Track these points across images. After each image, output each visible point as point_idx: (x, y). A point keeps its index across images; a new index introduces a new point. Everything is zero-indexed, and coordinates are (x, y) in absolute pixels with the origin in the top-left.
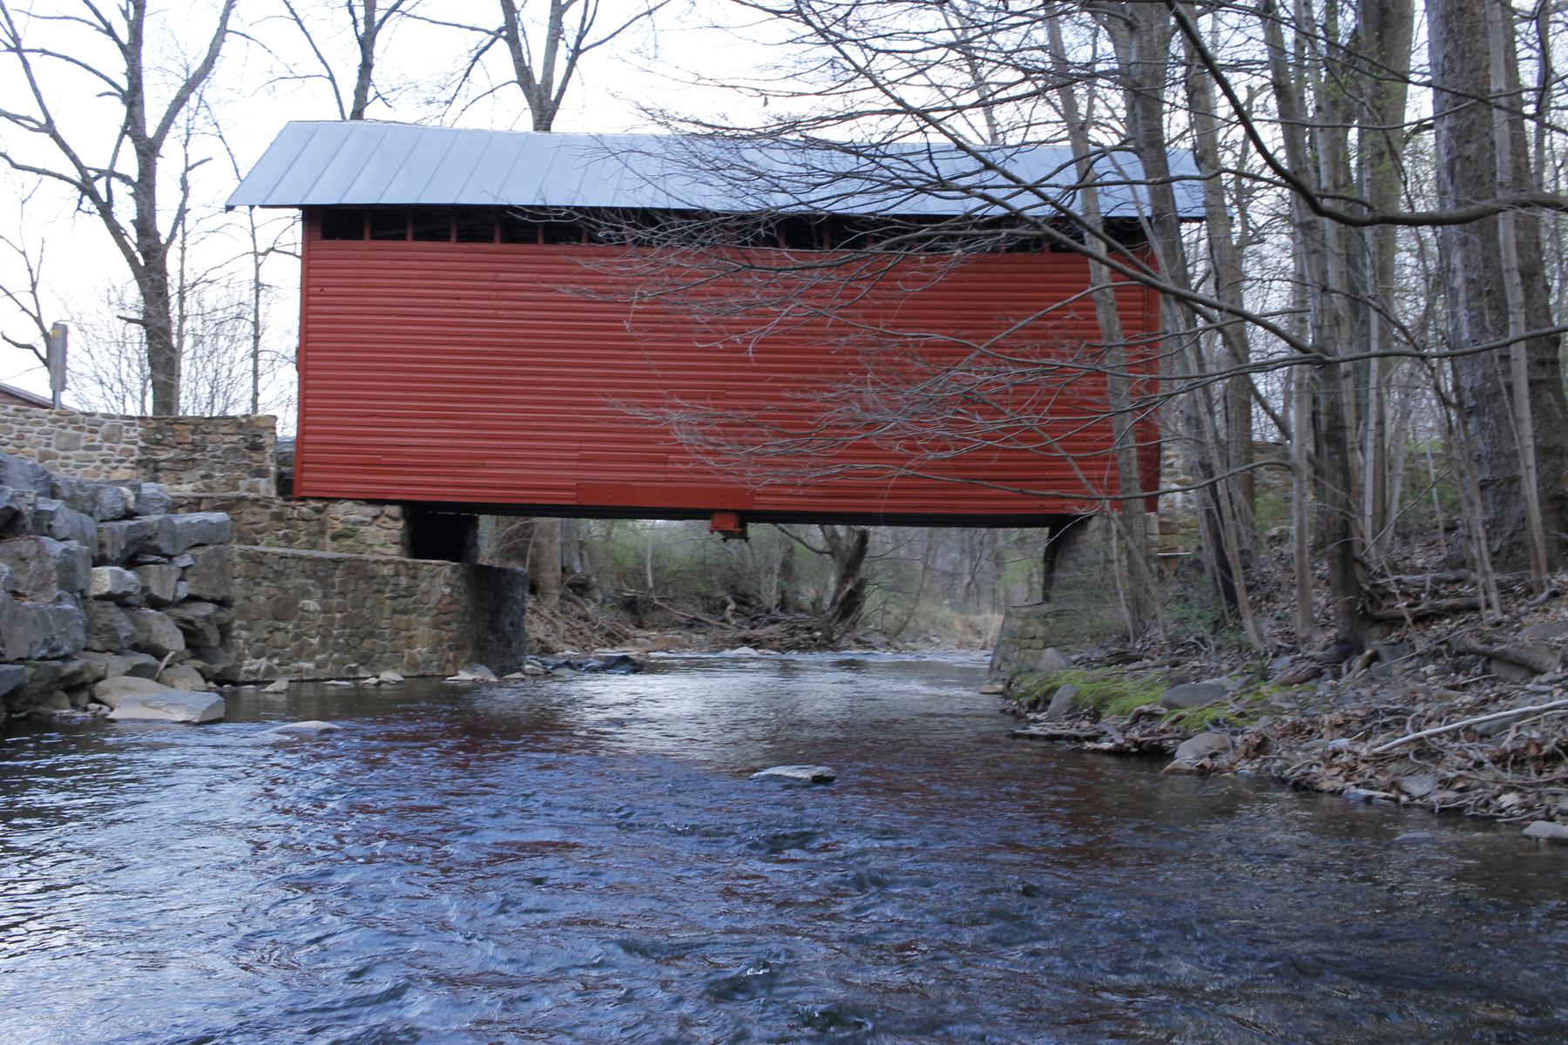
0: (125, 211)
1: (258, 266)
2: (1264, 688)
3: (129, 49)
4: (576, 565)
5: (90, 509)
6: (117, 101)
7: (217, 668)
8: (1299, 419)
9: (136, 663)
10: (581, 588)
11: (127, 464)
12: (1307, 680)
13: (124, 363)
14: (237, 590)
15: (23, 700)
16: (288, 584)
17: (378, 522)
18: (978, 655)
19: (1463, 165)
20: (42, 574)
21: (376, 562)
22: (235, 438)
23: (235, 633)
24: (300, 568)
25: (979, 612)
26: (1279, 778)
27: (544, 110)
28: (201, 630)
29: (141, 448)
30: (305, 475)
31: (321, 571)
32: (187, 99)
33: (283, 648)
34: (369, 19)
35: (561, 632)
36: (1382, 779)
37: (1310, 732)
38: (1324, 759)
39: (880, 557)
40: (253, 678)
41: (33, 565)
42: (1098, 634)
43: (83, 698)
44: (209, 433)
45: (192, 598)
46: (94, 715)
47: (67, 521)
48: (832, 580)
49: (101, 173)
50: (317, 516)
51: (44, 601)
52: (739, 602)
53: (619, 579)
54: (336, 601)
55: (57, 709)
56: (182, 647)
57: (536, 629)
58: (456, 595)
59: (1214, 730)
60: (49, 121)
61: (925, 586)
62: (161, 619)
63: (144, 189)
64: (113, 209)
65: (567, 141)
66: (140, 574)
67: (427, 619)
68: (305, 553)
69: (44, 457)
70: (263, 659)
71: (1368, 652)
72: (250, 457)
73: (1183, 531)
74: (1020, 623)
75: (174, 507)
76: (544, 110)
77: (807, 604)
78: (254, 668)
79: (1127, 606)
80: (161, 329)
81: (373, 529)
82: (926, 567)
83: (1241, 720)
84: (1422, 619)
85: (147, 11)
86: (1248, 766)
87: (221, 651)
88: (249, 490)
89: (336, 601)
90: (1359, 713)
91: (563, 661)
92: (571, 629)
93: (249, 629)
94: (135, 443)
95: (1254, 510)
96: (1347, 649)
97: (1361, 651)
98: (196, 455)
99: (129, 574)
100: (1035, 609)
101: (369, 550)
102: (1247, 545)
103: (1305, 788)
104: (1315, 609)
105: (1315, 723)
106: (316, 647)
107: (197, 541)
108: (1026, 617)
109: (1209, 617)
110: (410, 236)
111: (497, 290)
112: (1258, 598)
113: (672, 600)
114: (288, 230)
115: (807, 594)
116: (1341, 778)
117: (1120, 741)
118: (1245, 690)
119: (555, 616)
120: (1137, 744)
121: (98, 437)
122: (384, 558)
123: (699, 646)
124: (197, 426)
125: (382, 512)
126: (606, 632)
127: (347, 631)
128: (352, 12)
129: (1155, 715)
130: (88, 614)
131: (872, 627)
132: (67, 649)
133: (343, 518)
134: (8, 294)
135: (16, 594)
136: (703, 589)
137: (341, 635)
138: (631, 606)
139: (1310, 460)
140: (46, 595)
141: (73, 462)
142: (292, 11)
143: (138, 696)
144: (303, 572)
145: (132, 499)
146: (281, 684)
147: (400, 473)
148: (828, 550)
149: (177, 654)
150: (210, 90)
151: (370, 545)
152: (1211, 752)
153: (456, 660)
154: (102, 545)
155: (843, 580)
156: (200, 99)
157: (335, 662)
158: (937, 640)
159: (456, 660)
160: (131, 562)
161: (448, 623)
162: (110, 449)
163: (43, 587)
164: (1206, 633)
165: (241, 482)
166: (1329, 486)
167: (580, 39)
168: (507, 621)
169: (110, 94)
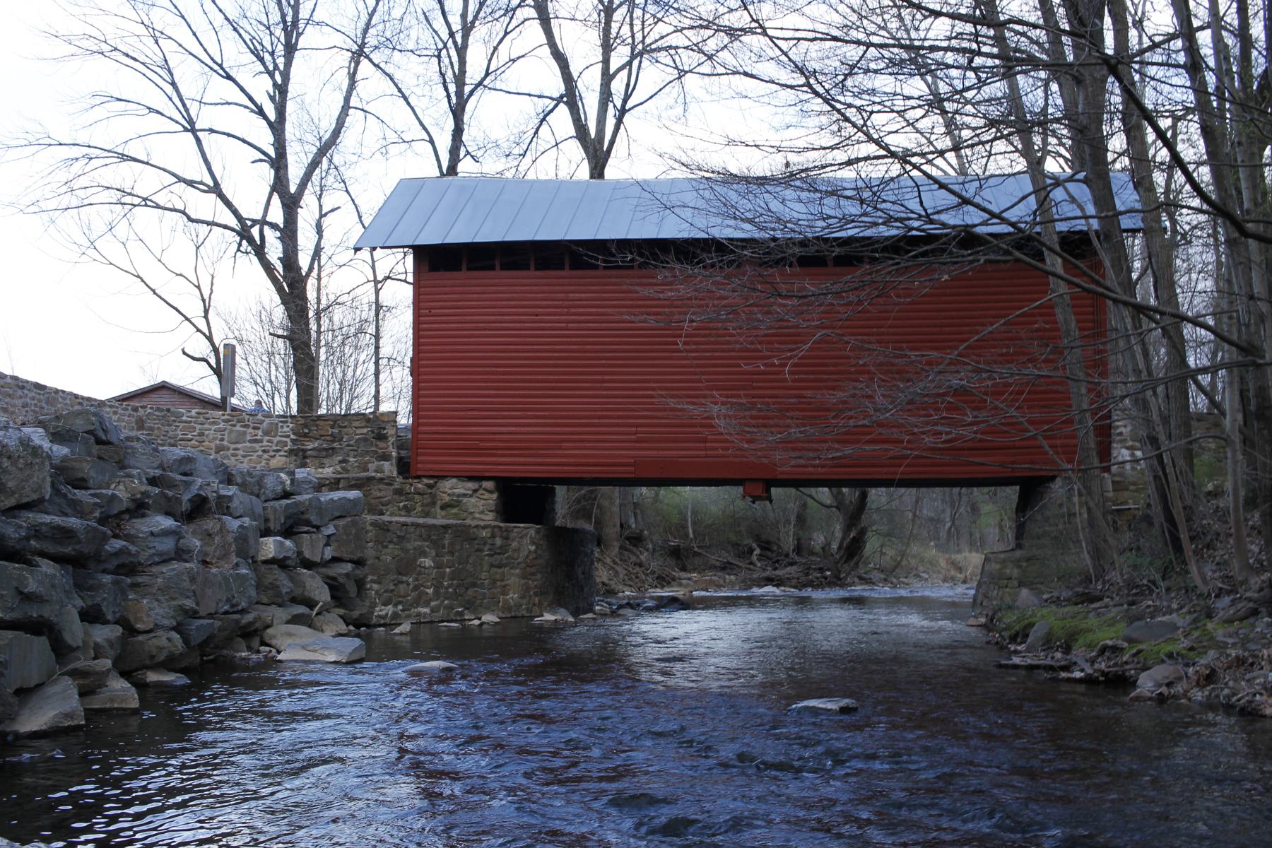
0: (274, 251)
1: (377, 292)
2: (1210, 626)
3: (275, 125)
5: (257, 492)
6: (266, 166)
7: (356, 614)
8: (1231, 400)
9: (296, 613)
10: (636, 540)
11: (282, 453)
12: (1246, 618)
13: (273, 367)
14: (370, 552)
15: (212, 645)
16: (409, 546)
18: (960, 589)
21: (477, 527)
22: (365, 431)
24: (418, 533)
25: (959, 552)
26: (1228, 704)
27: (598, 157)
28: (343, 585)
29: (292, 440)
30: (420, 458)
31: (434, 535)
32: (320, 162)
33: (404, 597)
34: (459, 93)
35: (621, 576)
37: (1252, 664)
39: (878, 509)
40: (382, 622)
41: (217, 539)
42: (1063, 576)
43: (255, 642)
44: (345, 427)
45: (335, 560)
46: (266, 657)
47: (241, 502)
48: (838, 530)
49: (255, 222)
50: (429, 491)
51: (226, 567)
52: (762, 548)
53: (665, 531)
54: (446, 559)
55: (238, 651)
56: (329, 599)
57: (602, 575)
58: (539, 552)
59: (1168, 662)
61: (915, 531)
62: (312, 577)
63: (289, 233)
64: (266, 250)
65: (618, 185)
66: (295, 542)
67: (517, 571)
68: (421, 521)
69: (219, 449)
70: (390, 606)
72: (376, 445)
73: (1132, 488)
74: (998, 566)
75: (319, 486)
76: (598, 157)
77: (818, 549)
78: (383, 613)
79: (1089, 553)
80: (303, 343)
81: (473, 500)
82: (915, 515)
83: (1191, 653)
85: (289, 95)
86: (1200, 693)
88: (376, 471)
91: (625, 602)
92: (629, 574)
94: (288, 436)
95: (1193, 471)
98: (335, 445)
99: (288, 543)
100: (1009, 554)
101: (470, 517)
102: (1189, 503)
103: (1250, 714)
104: (1250, 555)
105: (1257, 656)
107: (338, 514)
108: (1004, 561)
109: (1159, 563)
110: (498, 266)
112: (1200, 546)
113: (709, 547)
114: (404, 263)
115: (818, 539)
117: (1090, 671)
118: (1194, 626)
119: (615, 563)
120: (1103, 673)
121: (260, 433)
122: (482, 523)
123: (732, 585)
124: (335, 422)
125: (481, 486)
126: (656, 575)
127: (455, 582)
128: (446, 89)
129: (1118, 648)
130: (257, 575)
131: (872, 565)
133: (450, 492)
134: (187, 319)
135: (205, 563)
136: (733, 538)
137: (450, 586)
138: (676, 553)
139: (1241, 431)
140: (227, 563)
141: (241, 452)
142: (400, 90)
143: (298, 641)
144: (420, 536)
145: (289, 482)
146: (406, 627)
147: (495, 455)
148: (835, 504)
149: (325, 604)
150: (339, 156)
151: (472, 513)
152: (1167, 681)
153: (540, 604)
154: (267, 520)
155: (847, 528)
156: (331, 161)
157: (446, 607)
159: (540, 604)
160: (288, 532)
162: (269, 441)
163: (225, 556)
164: (1158, 577)
165: (370, 465)
166: (1259, 456)
167: (625, 101)
168: (579, 571)
169: (261, 160)
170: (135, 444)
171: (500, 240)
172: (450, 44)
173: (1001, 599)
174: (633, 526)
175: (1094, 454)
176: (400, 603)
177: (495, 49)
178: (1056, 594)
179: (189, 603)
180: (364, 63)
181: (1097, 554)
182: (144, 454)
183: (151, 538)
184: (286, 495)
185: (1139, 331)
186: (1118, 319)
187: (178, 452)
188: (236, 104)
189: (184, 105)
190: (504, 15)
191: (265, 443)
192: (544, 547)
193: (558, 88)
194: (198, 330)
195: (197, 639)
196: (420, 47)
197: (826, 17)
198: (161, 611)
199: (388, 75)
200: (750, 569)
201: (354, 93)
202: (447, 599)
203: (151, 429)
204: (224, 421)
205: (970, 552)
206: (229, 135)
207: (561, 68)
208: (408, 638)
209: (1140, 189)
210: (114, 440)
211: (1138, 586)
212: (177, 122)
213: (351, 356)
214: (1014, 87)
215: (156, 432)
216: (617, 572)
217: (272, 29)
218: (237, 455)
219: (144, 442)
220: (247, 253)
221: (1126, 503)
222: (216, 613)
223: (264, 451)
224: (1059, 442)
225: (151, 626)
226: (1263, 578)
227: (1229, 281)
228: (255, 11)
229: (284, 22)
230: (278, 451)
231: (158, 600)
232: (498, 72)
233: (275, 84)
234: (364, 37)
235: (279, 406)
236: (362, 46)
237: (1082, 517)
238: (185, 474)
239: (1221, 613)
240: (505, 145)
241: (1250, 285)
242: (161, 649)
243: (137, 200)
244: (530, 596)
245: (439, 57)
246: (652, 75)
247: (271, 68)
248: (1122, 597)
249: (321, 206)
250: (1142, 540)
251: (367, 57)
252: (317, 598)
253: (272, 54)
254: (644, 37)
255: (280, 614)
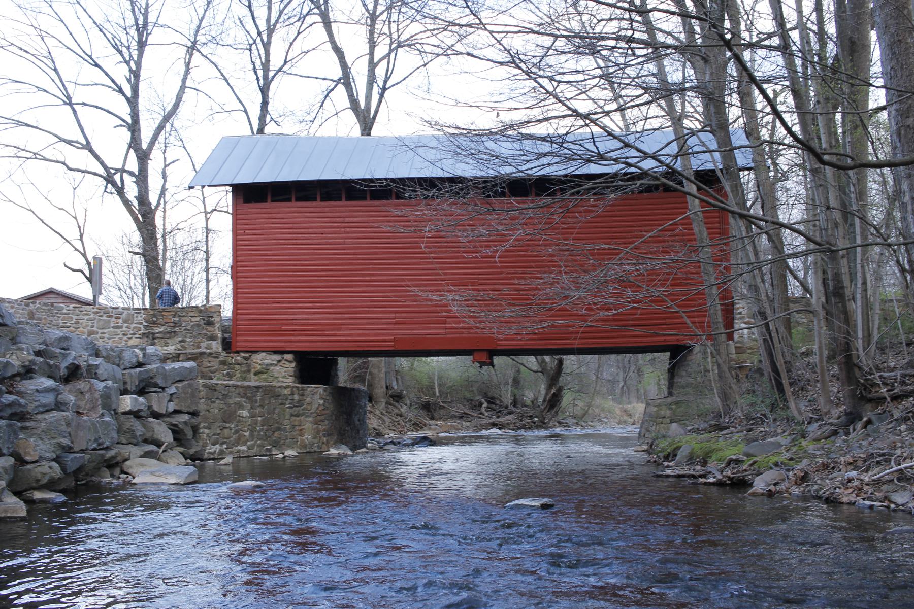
0: (131, 191)
1: (207, 220)
2: (804, 443)
3: (131, 100)
4: (394, 384)
5: (118, 363)
6: (125, 130)
7: (192, 451)
10: (398, 397)
12: (829, 437)
13: (132, 277)
14: (202, 406)
15: (84, 473)
16: (231, 401)
17: (281, 364)
18: (630, 428)
19: (906, 131)
20: (93, 401)
21: (280, 387)
22: (198, 319)
23: (201, 431)
24: (237, 392)
25: (629, 403)
27: (367, 123)
28: (182, 430)
29: (145, 326)
30: (238, 338)
31: (249, 393)
32: (164, 127)
34: (265, 77)
36: (879, 495)
37: (833, 468)
38: (843, 484)
40: (212, 457)
41: (87, 396)
42: (702, 414)
43: (117, 471)
44: (183, 316)
45: (176, 412)
46: (124, 481)
47: (106, 370)
48: (543, 388)
49: (117, 170)
50: (246, 362)
51: (94, 416)
52: (489, 402)
54: (258, 410)
55: (103, 478)
56: (172, 440)
57: (373, 422)
58: (327, 405)
60: (88, 142)
61: (597, 389)
62: (159, 424)
63: (142, 178)
64: (125, 191)
67: (311, 419)
68: (239, 383)
69: (91, 333)
71: (865, 419)
72: (206, 329)
73: (749, 351)
74: (655, 409)
75: (164, 360)
76: (367, 123)
77: (528, 402)
78: (212, 450)
80: (153, 257)
81: (278, 368)
82: (597, 377)
84: (896, 398)
85: (141, 78)
86: (797, 490)
87: (194, 442)
88: (206, 348)
89: (258, 410)
90: (862, 455)
93: (209, 429)
94: (141, 324)
95: (791, 338)
96: (852, 418)
97: (861, 419)
98: (176, 329)
99: (141, 399)
102: (788, 359)
103: (832, 502)
106: (247, 437)
107: (178, 379)
108: (659, 405)
109: (768, 401)
110: (293, 199)
111: (344, 228)
112: (797, 389)
113: (450, 402)
114: (225, 198)
115: (529, 396)
116: (854, 495)
117: (720, 477)
119: (383, 414)
120: (730, 478)
121: (120, 321)
122: (284, 385)
123: (467, 428)
126: (413, 422)
127: (265, 427)
128: (256, 73)
129: (740, 461)
130: (118, 423)
131: (567, 414)
132: (107, 443)
133: (260, 362)
134: (67, 241)
135: (78, 413)
136: (468, 396)
139: (823, 307)
141: (107, 336)
142: (222, 74)
143: (148, 469)
145: (141, 356)
146: (228, 459)
148: (540, 370)
150: (178, 121)
152: (774, 482)
154: (125, 383)
155: (550, 387)
156: (172, 126)
157: (259, 446)
158: (605, 420)
160: (141, 392)
161: (322, 421)
163: (93, 408)
164: (767, 411)
167: (385, 82)
168: (356, 419)
169: (121, 126)
170: (25, 326)
171: (295, 179)
172: (258, 40)
173: (658, 432)
174: (396, 388)
175: (722, 326)
176: (225, 443)
177: (291, 44)
178: (696, 426)
179: (66, 441)
180: (196, 54)
181: (725, 397)
182: (31, 334)
183: (36, 394)
184: (140, 365)
185: (751, 234)
186: (737, 227)
187: (59, 333)
188: (102, 85)
189: (64, 85)
190: (298, 20)
191: (124, 329)
192: (330, 402)
193: (338, 73)
194: (76, 249)
195: (72, 467)
196: (237, 42)
197: (524, 15)
198: (44, 447)
199: (213, 63)
200: (480, 418)
201: (189, 76)
202: (259, 439)
203: (40, 319)
204: (94, 313)
205: (637, 403)
206: (97, 107)
207: (339, 58)
208: (230, 468)
209: (750, 138)
210: (8, 322)
211: (753, 419)
212: (58, 98)
213: (189, 268)
214: (661, 68)
215: (43, 321)
216: (384, 421)
217: (128, 30)
218: (103, 338)
219: (32, 326)
220: (111, 193)
221: (746, 362)
222: (87, 449)
223: (124, 335)
224: (696, 319)
225: (36, 458)
226: (840, 409)
227: (813, 200)
228: (116, 17)
229: (137, 25)
230: (134, 334)
231: (42, 439)
232: (294, 61)
233: (131, 70)
234: (196, 35)
235: (138, 304)
236: (194, 43)
237: (713, 375)
238: (63, 349)
239: (812, 434)
240: (298, 114)
241: (827, 198)
242: (44, 474)
243: (30, 155)
244: (320, 437)
245: (250, 50)
246: (406, 60)
247: (128, 59)
248: (742, 426)
249: (165, 158)
250: (756, 386)
251: (198, 51)
252: (163, 440)
253: (128, 48)
254: (399, 36)
255: (135, 451)
